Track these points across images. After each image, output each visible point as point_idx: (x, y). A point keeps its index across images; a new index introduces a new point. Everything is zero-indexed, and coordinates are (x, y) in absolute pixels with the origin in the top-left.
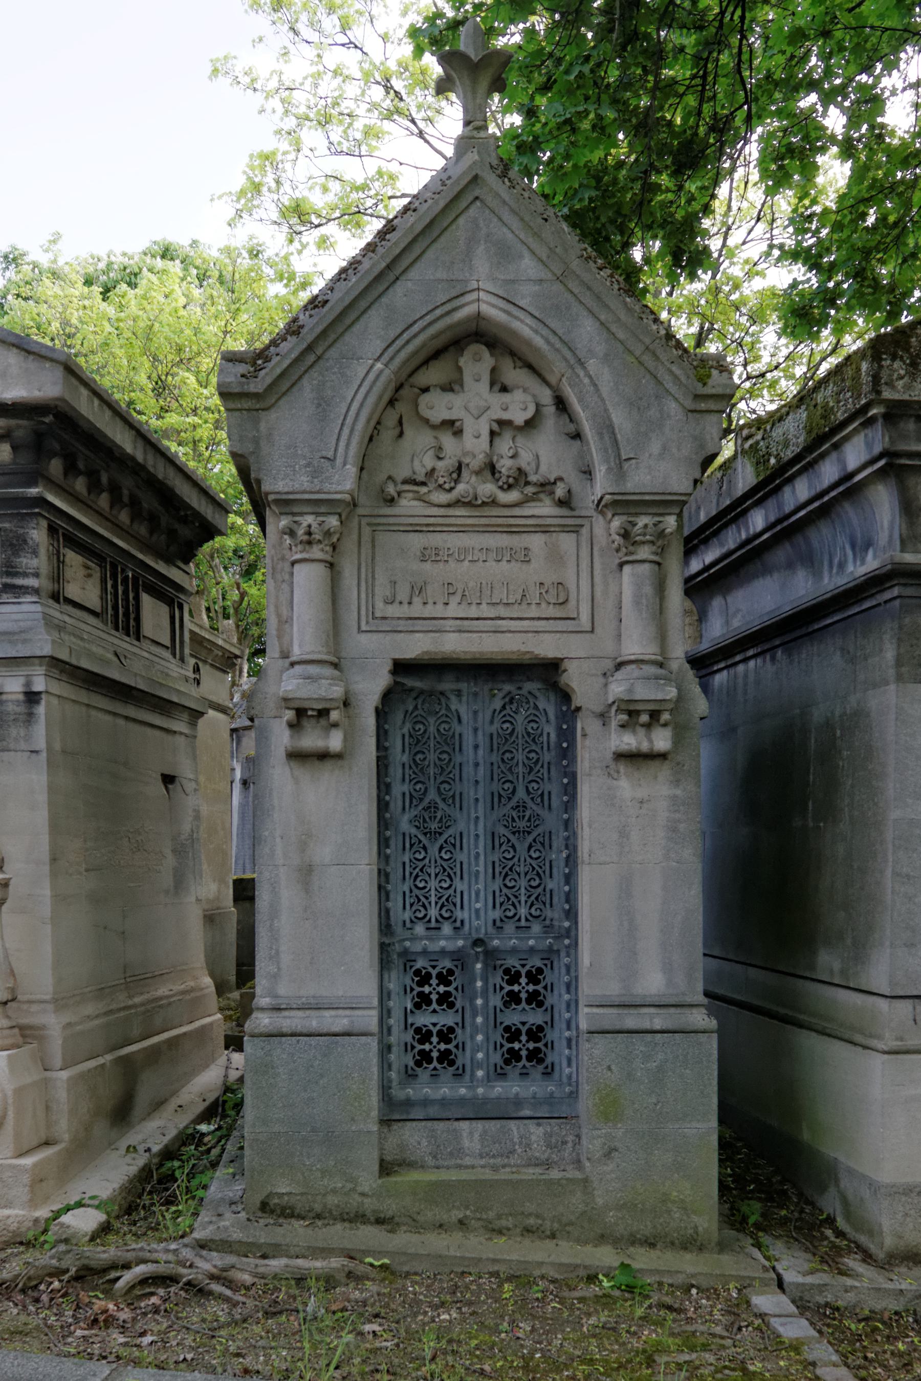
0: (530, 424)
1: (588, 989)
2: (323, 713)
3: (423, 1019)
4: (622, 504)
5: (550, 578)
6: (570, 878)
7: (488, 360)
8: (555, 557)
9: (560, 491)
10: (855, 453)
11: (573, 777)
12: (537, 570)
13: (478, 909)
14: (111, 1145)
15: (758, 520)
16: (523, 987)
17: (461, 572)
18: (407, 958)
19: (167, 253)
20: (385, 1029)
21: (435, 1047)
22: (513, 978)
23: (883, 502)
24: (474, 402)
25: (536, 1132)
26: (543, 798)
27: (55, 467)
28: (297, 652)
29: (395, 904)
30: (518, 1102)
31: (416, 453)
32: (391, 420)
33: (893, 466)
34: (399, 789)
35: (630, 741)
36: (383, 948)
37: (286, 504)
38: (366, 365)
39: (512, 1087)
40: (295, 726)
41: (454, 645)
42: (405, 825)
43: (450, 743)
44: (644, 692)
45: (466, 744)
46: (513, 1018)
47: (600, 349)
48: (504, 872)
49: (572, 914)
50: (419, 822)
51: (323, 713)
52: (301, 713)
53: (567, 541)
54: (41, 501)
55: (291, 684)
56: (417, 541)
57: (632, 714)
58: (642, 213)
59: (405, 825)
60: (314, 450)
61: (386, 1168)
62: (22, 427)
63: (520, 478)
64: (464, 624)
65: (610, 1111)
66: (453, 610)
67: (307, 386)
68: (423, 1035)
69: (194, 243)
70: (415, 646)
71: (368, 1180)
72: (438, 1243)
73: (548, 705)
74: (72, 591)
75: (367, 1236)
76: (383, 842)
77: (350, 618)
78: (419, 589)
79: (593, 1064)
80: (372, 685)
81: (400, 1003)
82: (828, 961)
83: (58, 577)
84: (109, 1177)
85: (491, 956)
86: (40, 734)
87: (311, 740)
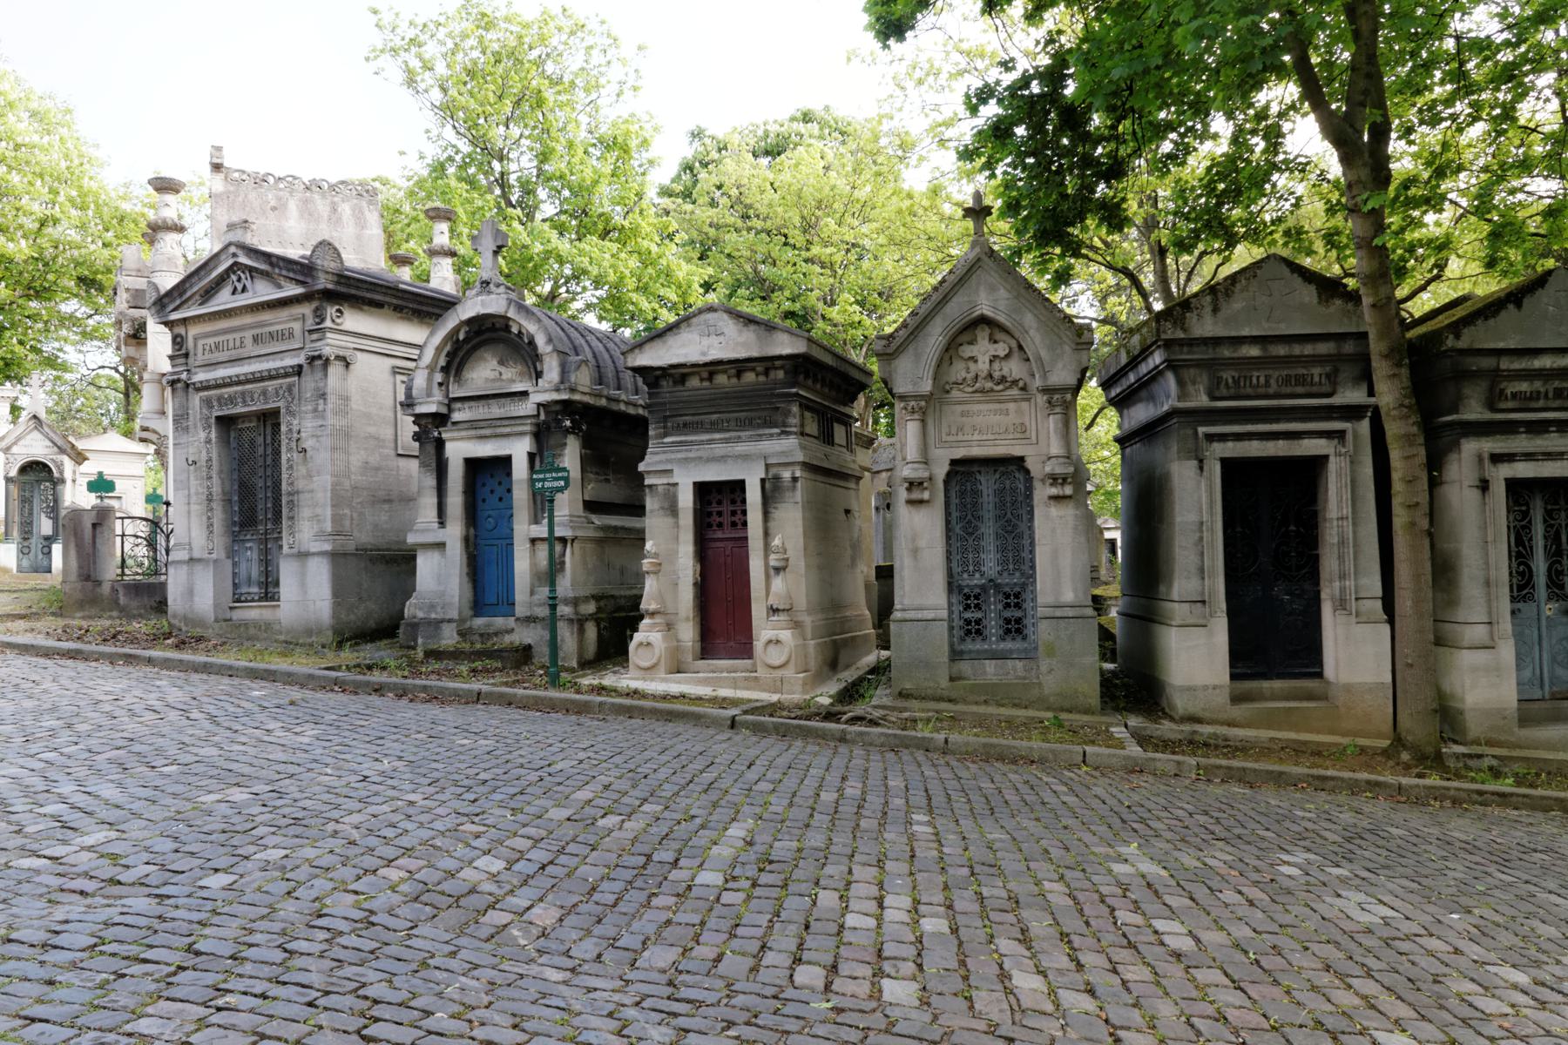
0: (1007, 356)
1: (1040, 600)
2: (921, 484)
3: (968, 615)
4: (1047, 390)
5: (1018, 421)
6: (1032, 552)
7: (987, 331)
8: (1019, 412)
9: (1021, 384)
10: (1157, 358)
11: (1032, 508)
12: (1012, 418)
13: (991, 564)
14: (830, 678)
15: (1132, 378)
16: (1012, 600)
17: (978, 420)
18: (960, 588)
19: (807, 118)
20: (950, 620)
21: (973, 627)
22: (1007, 596)
23: (1170, 380)
24: (983, 350)
25: (1019, 664)
26: (1019, 517)
27: (801, 377)
28: (909, 458)
29: (954, 564)
30: (1011, 651)
31: (958, 371)
32: (947, 357)
33: (1171, 365)
34: (955, 514)
35: (1054, 491)
36: (950, 584)
37: (902, 398)
38: (935, 338)
39: (1008, 645)
40: (908, 490)
41: (976, 452)
42: (958, 530)
43: (976, 493)
44: (1059, 470)
45: (986, 496)
46: (1008, 614)
47: (1035, 325)
48: (1002, 549)
49: (1033, 567)
50: (964, 529)
51: (921, 484)
52: (911, 484)
53: (1025, 405)
54: (797, 394)
55: (907, 472)
56: (959, 408)
57: (1055, 479)
58: (1082, 206)
59: (958, 530)
60: (913, 375)
61: (952, 679)
62: (788, 364)
63: (1003, 379)
64: (980, 443)
65: (1051, 652)
66: (976, 437)
67: (911, 349)
68: (968, 622)
69: (827, 108)
70: (959, 453)
71: (944, 683)
72: (974, 708)
73: (1020, 476)
74: (808, 430)
75: (943, 705)
76: (948, 538)
77: (931, 441)
78: (961, 429)
79: (1043, 632)
80: (941, 471)
81: (957, 608)
82: (1162, 588)
83: (802, 425)
84: (833, 687)
85: (997, 587)
86: (798, 495)
87: (916, 495)
